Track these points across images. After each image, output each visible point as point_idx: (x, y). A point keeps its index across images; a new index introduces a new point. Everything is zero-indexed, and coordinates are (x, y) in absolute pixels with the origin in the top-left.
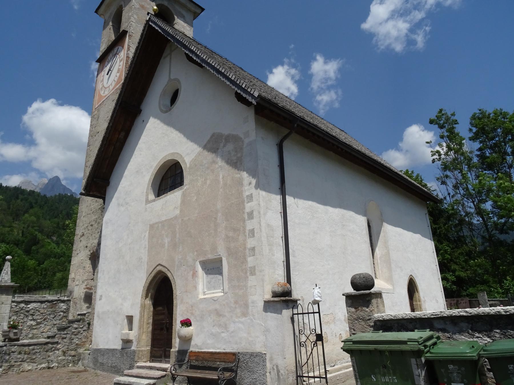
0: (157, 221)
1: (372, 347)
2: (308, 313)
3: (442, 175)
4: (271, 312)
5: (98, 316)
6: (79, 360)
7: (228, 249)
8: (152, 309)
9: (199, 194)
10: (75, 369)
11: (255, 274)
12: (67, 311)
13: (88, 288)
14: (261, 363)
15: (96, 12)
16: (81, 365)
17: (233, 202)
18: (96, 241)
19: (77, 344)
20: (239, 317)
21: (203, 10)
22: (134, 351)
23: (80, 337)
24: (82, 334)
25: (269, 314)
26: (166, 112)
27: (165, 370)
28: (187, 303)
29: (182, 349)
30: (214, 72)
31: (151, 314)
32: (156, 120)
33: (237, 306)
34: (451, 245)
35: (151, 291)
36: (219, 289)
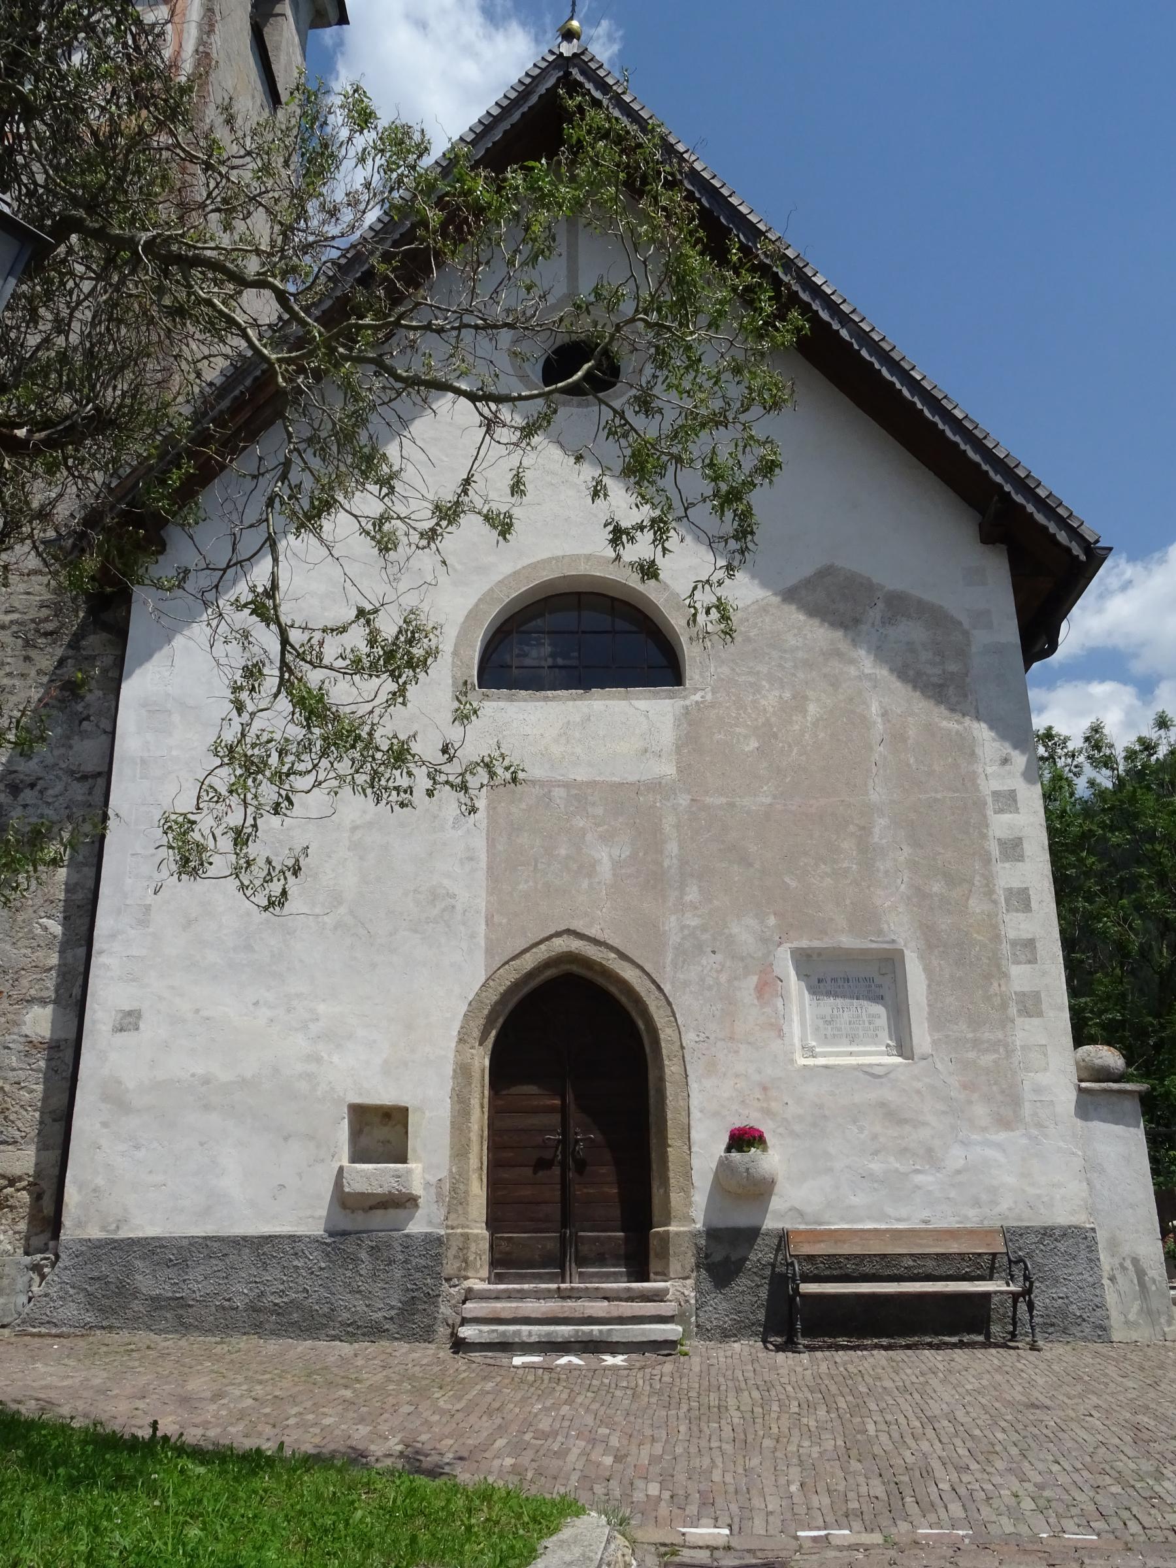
9: (775, 736)
11: (1040, 1014)
17: (939, 796)
20: (984, 1129)
22: (435, 1243)
29: (723, 1222)
33: (975, 1096)
34: (20, 1383)
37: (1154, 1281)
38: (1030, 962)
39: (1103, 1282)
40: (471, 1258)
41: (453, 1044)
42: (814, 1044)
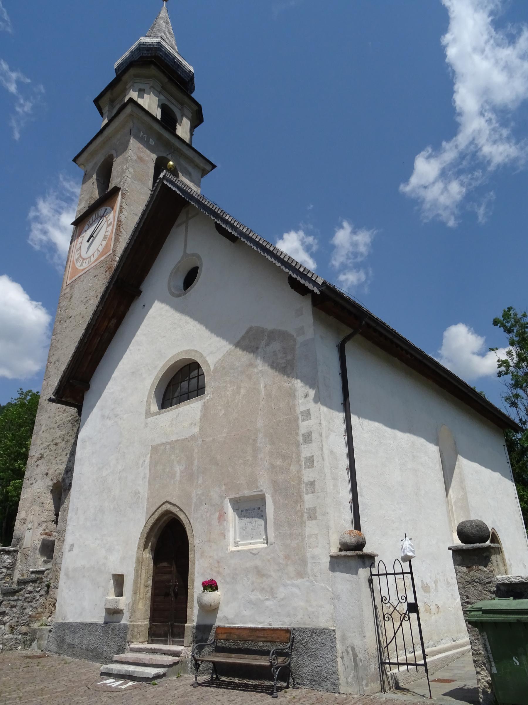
0: (164, 441)
1: (513, 618)
2: (387, 574)
3: (511, 395)
4: (341, 572)
5: (67, 575)
6: (33, 640)
7: (275, 483)
8: (152, 565)
9: (230, 407)
10: (28, 652)
11: (316, 519)
12: (11, 567)
13: (46, 534)
14: (329, 644)
15: (75, 160)
16: (36, 648)
17: (281, 419)
18: (63, 467)
19: (30, 616)
20: (292, 578)
21: (214, 166)
22: (126, 627)
23: (35, 606)
24: (38, 600)
25: (338, 574)
26: (179, 296)
27: (176, 654)
28: (210, 557)
29: (202, 623)
30: (259, 250)
31: (151, 572)
32: (163, 305)
33: (289, 562)
35: (153, 539)
36: (260, 538)
37: (361, 660)
38: (312, 493)
39: (337, 659)
40: (135, 634)
41: (136, 550)
42: (239, 540)
